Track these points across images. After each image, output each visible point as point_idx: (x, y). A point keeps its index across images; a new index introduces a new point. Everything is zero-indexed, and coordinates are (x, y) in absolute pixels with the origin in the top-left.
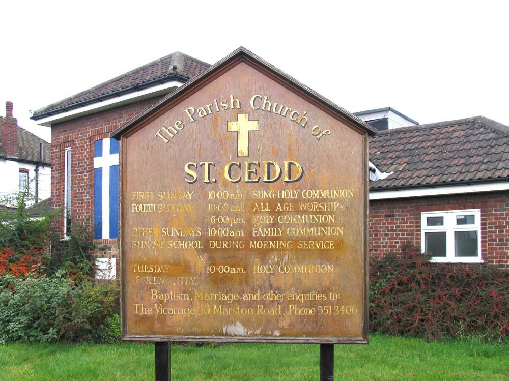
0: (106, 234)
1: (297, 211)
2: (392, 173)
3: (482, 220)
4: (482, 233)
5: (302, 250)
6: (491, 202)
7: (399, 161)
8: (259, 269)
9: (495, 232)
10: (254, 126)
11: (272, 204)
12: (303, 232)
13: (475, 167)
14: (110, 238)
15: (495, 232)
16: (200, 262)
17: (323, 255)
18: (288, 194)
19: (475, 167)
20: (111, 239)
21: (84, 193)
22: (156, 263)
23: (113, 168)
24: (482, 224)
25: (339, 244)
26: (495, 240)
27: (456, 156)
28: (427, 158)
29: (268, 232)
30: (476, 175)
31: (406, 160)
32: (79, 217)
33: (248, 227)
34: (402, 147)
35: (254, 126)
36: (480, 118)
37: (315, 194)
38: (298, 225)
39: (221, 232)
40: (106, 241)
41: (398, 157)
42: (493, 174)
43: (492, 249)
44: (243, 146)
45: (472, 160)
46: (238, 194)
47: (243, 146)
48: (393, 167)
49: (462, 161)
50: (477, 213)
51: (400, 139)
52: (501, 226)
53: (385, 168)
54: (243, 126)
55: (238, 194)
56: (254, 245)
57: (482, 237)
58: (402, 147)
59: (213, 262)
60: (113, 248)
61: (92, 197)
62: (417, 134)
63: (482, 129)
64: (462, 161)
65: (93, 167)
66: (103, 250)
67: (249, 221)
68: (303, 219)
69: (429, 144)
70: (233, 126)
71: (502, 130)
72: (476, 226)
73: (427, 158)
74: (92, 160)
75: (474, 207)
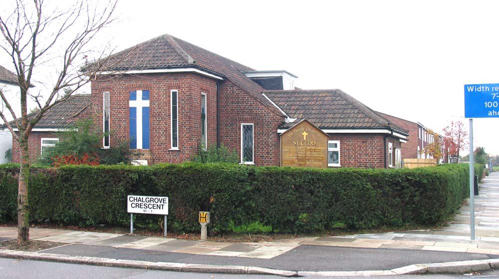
0: (139, 145)
1: (315, 151)
2: (296, 119)
3: (341, 146)
4: (341, 152)
5: (316, 159)
6: (345, 138)
7: (298, 112)
8: (308, 163)
9: (346, 152)
10: (307, 134)
11: (310, 149)
12: (316, 156)
13: (337, 120)
14: (143, 148)
15: (346, 152)
16: (296, 161)
17: (320, 160)
18: (313, 148)
19: (337, 120)
20: (144, 149)
21: (121, 121)
22: (288, 161)
23: (144, 109)
24: (341, 148)
25: (323, 158)
26: (346, 156)
27: (328, 112)
28: (313, 112)
29: (309, 155)
30: (338, 124)
31: (302, 112)
32: (117, 135)
33: (306, 154)
34: (298, 103)
35: (307, 134)
36: (338, 90)
37: (318, 148)
38: (315, 154)
39: (300, 155)
40: (140, 150)
41: (297, 109)
42: (346, 125)
43: (346, 160)
44: (305, 138)
45: (336, 116)
46: (304, 148)
47: (305, 138)
48: (296, 115)
49: (331, 116)
50: (338, 142)
51: (296, 97)
52: (349, 150)
53: (292, 116)
54: (305, 134)
55: (304, 148)
56: (307, 158)
57: (341, 154)
58: (298, 103)
59: (299, 161)
60: (145, 154)
61: (128, 124)
62: (306, 95)
63: (340, 98)
64: (331, 116)
65: (128, 106)
66: (138, 155)
67: (306, 153)
68: (316, 153)
69: (313, 103)
70: (303, 134)
71: (349, 100)
72: (338, 149)
73: (313, 112)
74: (128, 102)
75: (337, 140)
